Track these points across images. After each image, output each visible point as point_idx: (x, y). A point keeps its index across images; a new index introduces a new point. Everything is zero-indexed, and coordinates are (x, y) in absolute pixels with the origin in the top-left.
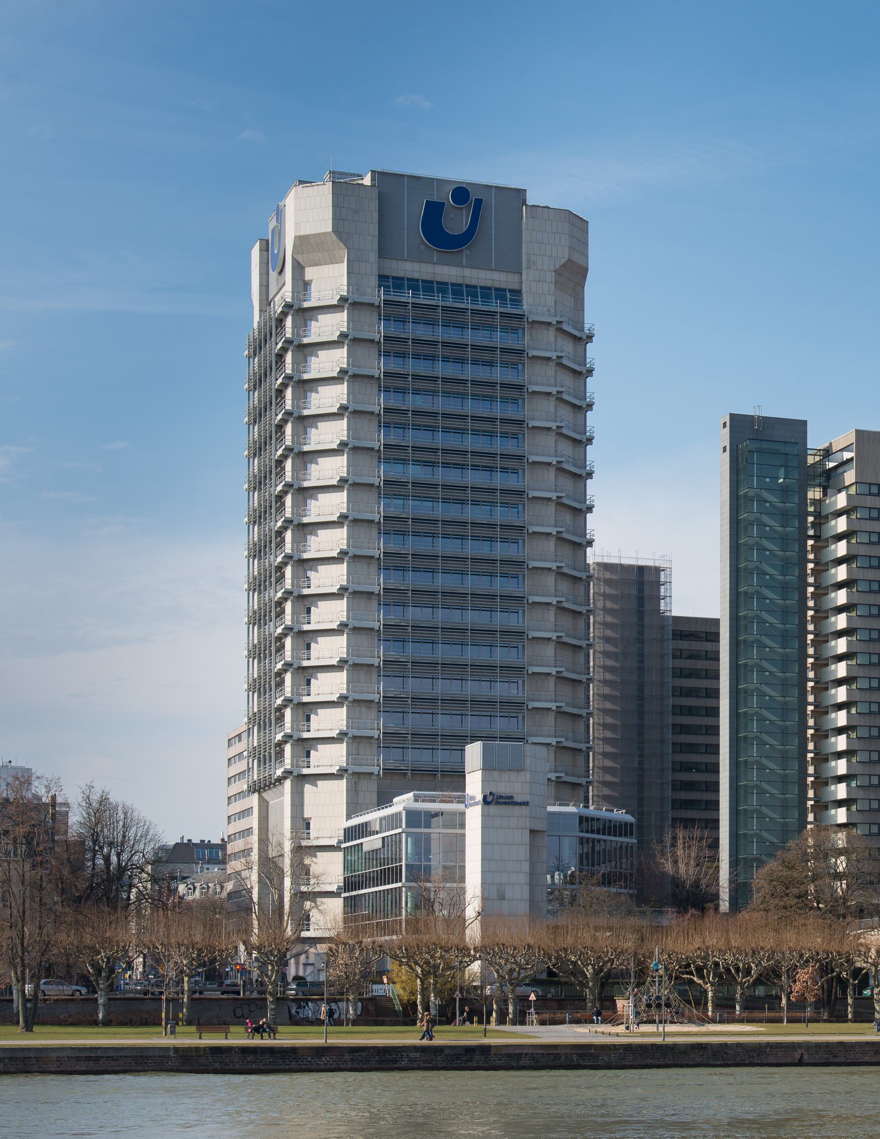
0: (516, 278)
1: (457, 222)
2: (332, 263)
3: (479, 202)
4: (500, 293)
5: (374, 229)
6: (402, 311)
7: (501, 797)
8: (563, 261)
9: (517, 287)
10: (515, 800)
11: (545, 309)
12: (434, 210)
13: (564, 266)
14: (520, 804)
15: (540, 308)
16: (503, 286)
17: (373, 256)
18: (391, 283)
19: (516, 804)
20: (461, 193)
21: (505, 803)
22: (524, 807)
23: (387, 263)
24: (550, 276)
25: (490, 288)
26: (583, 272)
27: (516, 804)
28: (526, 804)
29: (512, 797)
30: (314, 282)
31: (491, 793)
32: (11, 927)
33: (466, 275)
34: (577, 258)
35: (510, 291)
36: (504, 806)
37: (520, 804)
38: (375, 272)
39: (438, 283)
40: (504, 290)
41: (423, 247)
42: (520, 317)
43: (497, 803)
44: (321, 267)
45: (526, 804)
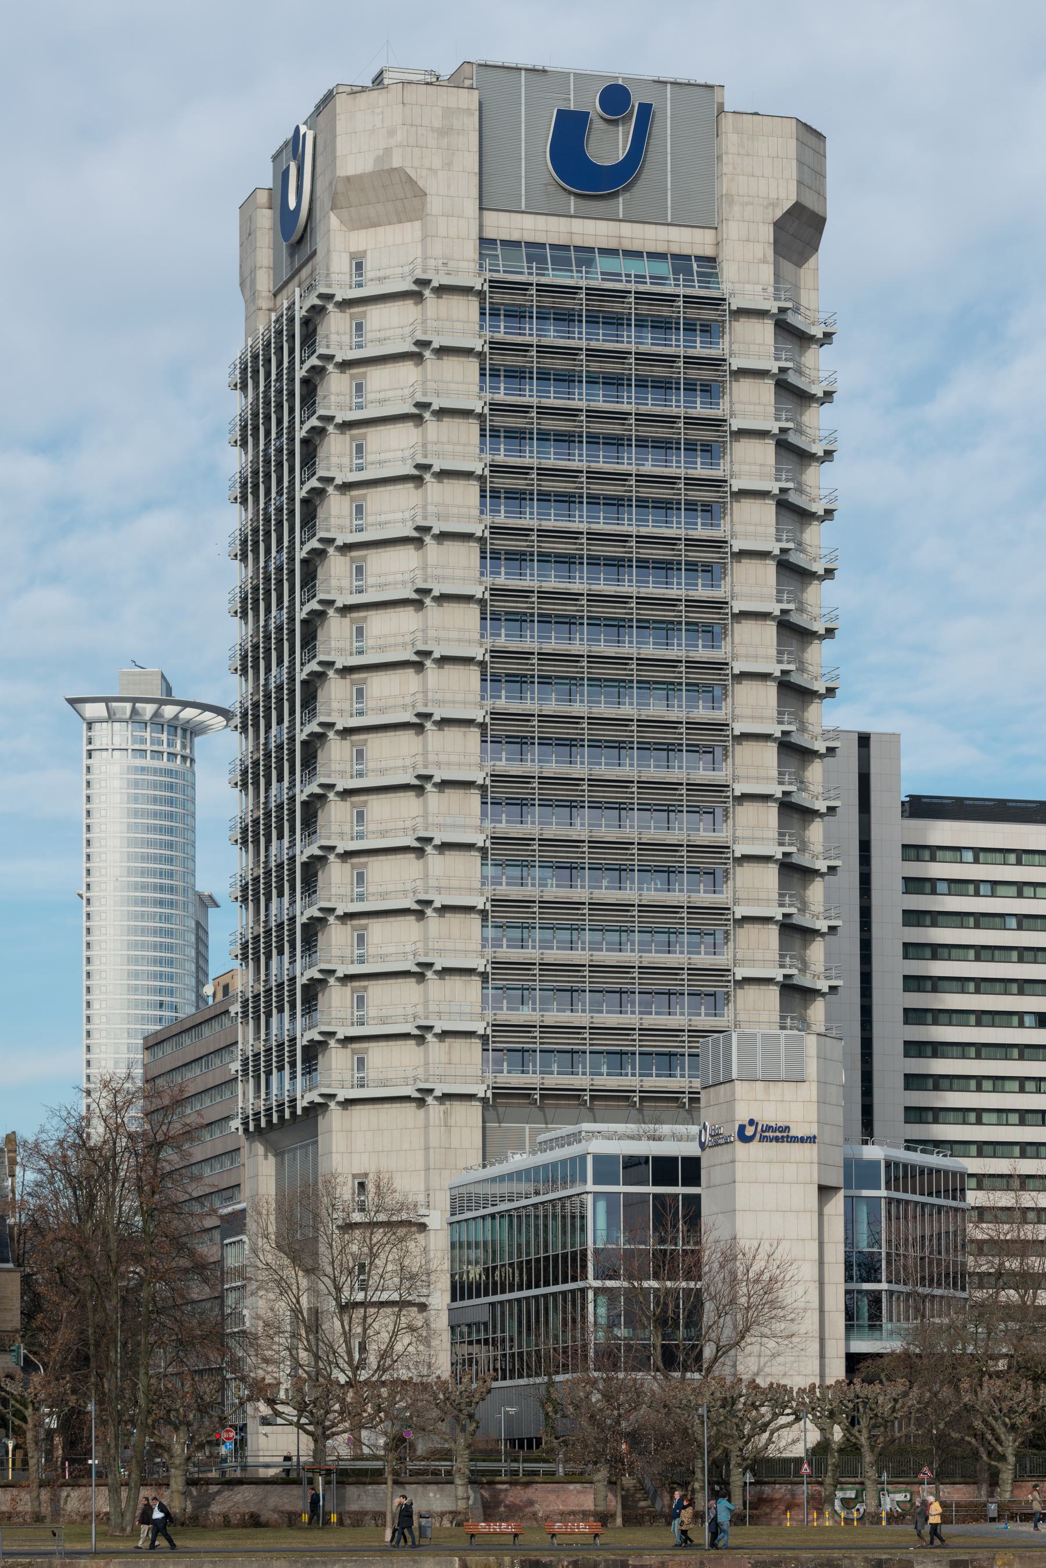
0: (709, 235)
1: (608, 146)
2: (400, 222)
3: (645, 110)
4: (681, 261)
5: (472, 162)
6: (519, 299)
7: (769, 1128)
8: (787, 205)
9: (709, 252)
10: (793, 1133)
11: (759, 288)
12: (570, 128)
13: (789, 213)
14: (802, 1140)
15: (748, 287)
16: (686, 251)
17: (471, 206)
18: (499, 252)
19: (795, 1139)
20: (615, 98)
21: (777, 1139)
22: (807, 1145)
23: (490, 217)
24: (767, 233)
25: (566, 248)
26: (818, 222)
27: (795, 1139)
28: (812, 1139)
29: (788, 1128)
30: (369, 253)
31: (752, 1122)
32: (415, 1206)
33: (623, 234)
34: (810, 202)
35: (699, 258)
36: (774, 1143)
37: (802, 1140)
38: (475, 235)
39: (578, 249)
40: (688, 257)
41: (552, 188)
42: (717, 302)
43: (763, 1139)
44: (380, 229)
45: (812, 1139)
